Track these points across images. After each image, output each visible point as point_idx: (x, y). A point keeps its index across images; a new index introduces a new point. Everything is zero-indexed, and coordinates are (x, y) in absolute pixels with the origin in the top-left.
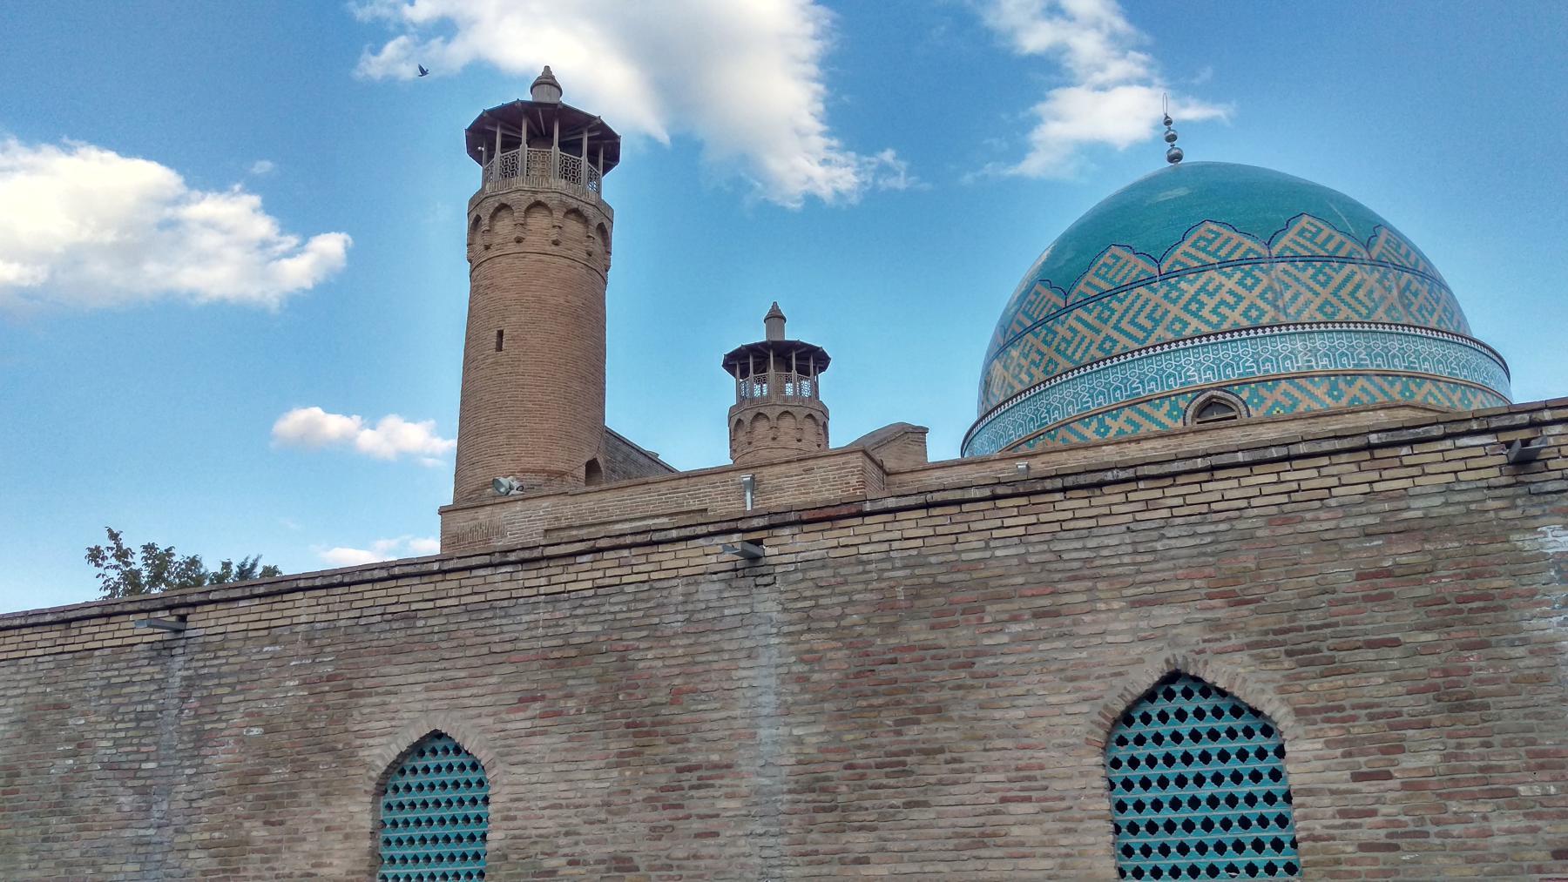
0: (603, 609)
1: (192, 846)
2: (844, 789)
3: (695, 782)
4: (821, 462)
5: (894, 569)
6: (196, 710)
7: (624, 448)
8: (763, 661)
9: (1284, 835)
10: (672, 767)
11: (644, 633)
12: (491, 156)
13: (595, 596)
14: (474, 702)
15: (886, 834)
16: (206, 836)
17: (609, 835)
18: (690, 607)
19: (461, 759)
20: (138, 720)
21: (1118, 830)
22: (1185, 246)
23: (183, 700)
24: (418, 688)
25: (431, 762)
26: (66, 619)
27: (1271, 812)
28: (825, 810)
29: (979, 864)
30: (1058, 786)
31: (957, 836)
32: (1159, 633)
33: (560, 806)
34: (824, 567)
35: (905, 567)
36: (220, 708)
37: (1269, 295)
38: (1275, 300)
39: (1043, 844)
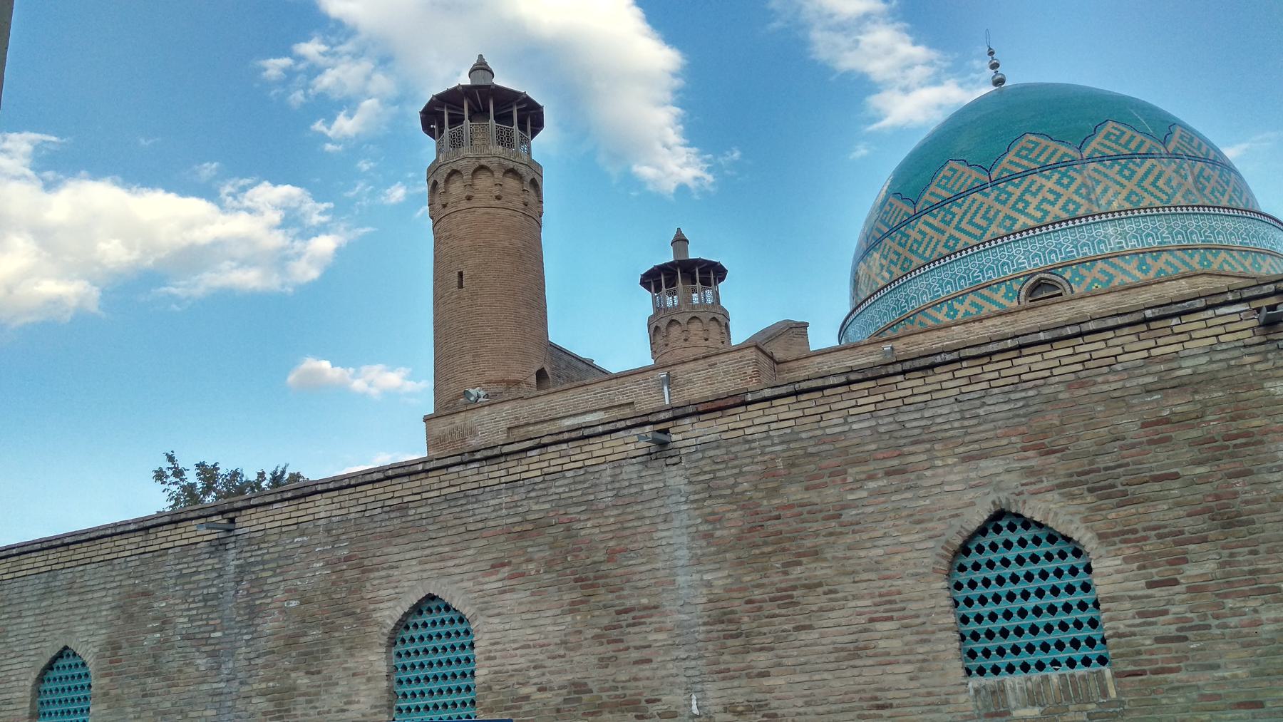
0: (551, 491)
1: (253, 694)
2: (746, 619)
3: (631, 621)
4: (722, 358)
5: (773, 445)
6: (248, 590)
7: (566, 357)
8: (676, 523)
9: (1094, 633)
10: (612, 610)
11: (583, 508)
12: (441, 132)
13: (544, 481)
14: (457, 570)
15: (780, 652)
16: (263, 685)
17: (568, 667)
18: (617, 485)
19: (451, 615)
20: (205, 600)
21: (963, 638)
22: (1011, 156)
23: (238, 583)
24: (414, 562)
25: (428, 618)
26: (145, 527)
27: (1084, 616)
28: (732, 637)
29: (856, 671)
30: (913, 606)
31: (837, 650)
32: (985, 481)
33: (529, 647)
34: (718, 447)
35: (782, 443)
36: (266, 588)
37: (1083, 191)
38: (1089, 194)
39: (904, 653)
